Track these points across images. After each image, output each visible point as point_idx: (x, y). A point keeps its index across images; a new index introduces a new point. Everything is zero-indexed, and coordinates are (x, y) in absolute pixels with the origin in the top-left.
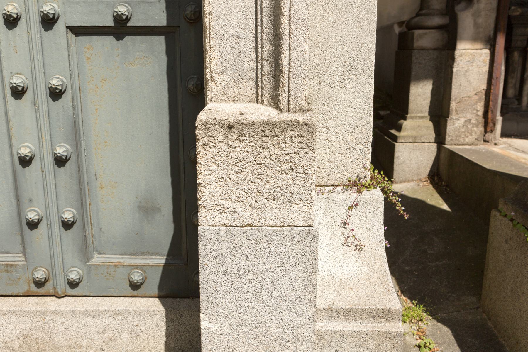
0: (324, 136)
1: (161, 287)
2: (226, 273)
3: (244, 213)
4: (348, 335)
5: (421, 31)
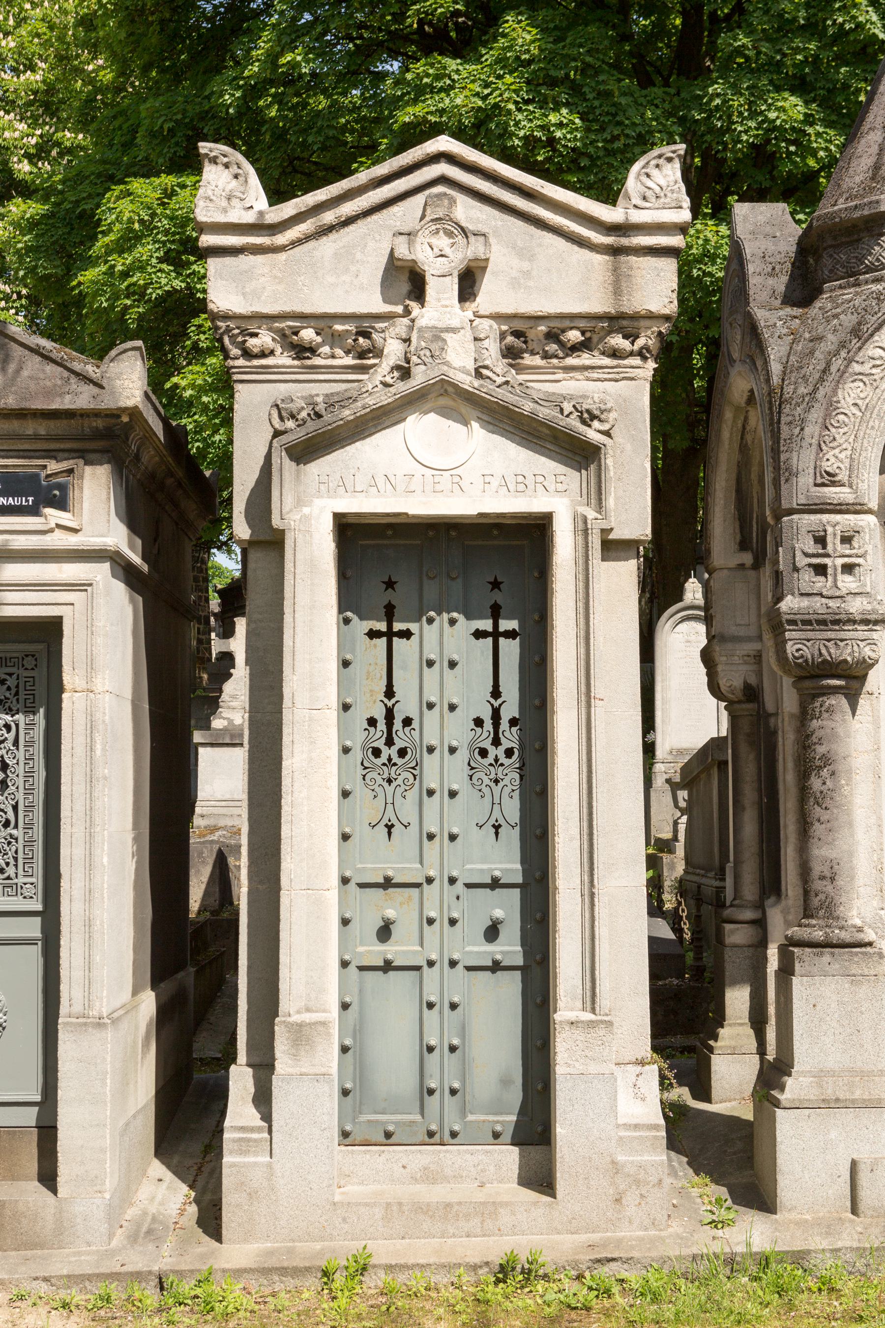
0: (619, 1031)
1: (513, 1136)
2: (570, 1100)
3: (579, 1067)
4: (636, 1138)
5: (732, 926)
